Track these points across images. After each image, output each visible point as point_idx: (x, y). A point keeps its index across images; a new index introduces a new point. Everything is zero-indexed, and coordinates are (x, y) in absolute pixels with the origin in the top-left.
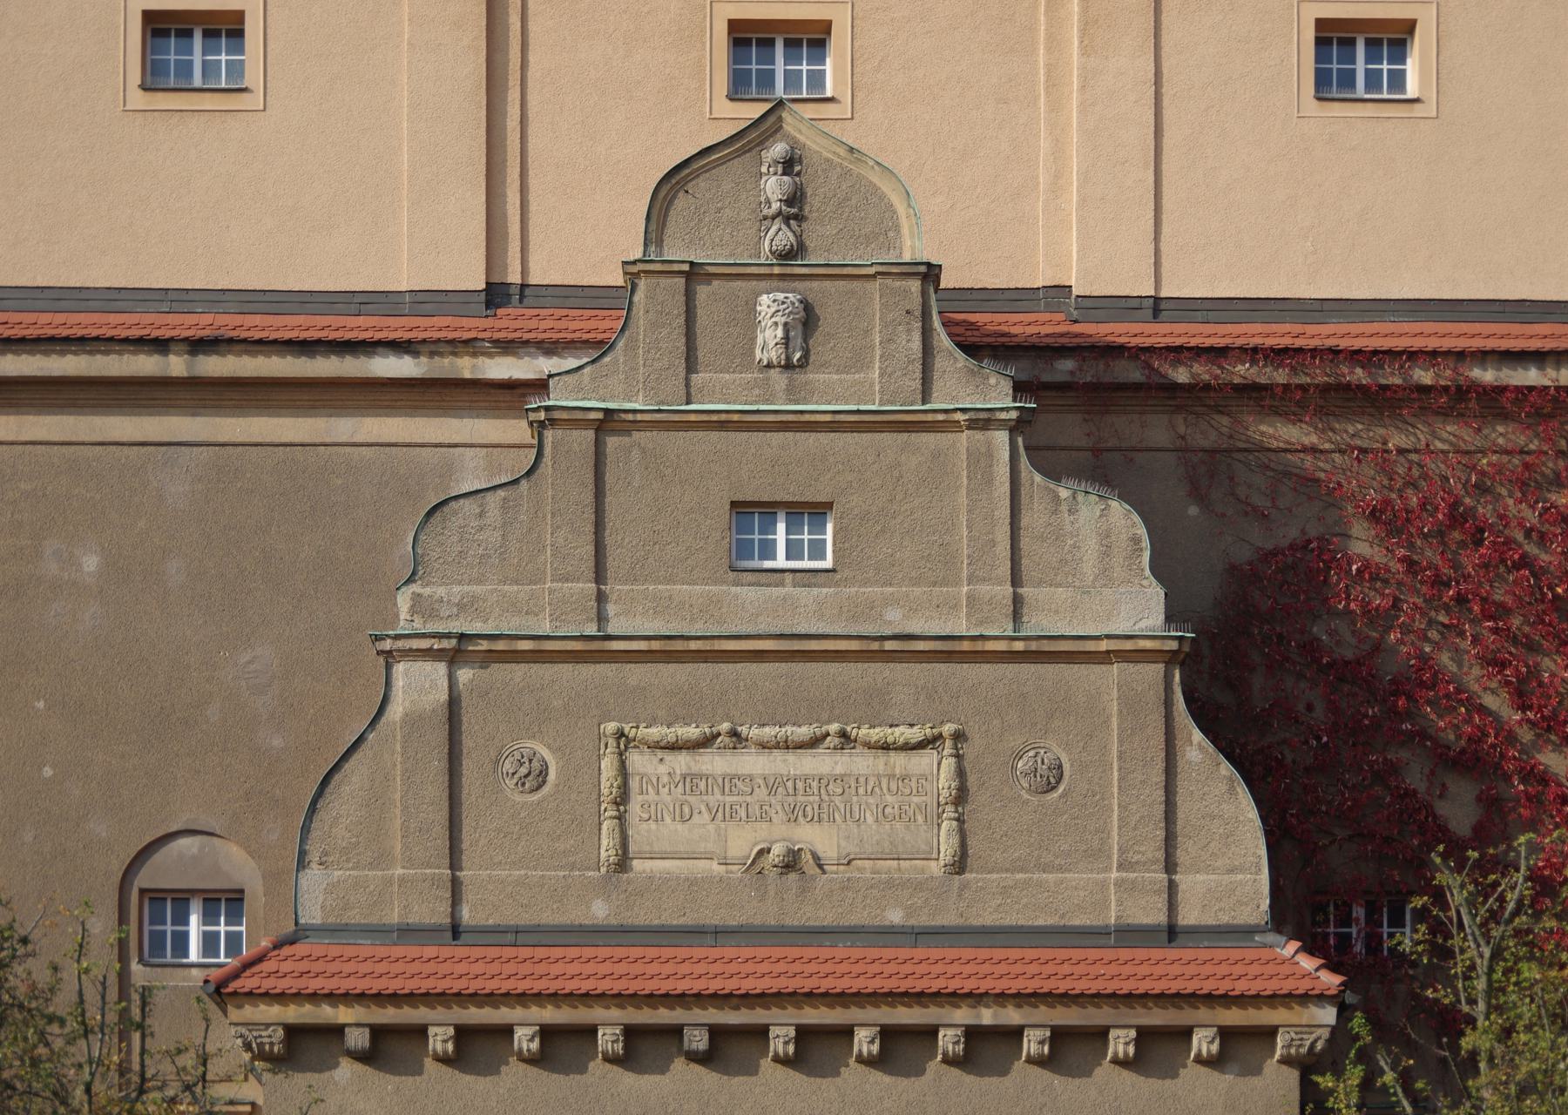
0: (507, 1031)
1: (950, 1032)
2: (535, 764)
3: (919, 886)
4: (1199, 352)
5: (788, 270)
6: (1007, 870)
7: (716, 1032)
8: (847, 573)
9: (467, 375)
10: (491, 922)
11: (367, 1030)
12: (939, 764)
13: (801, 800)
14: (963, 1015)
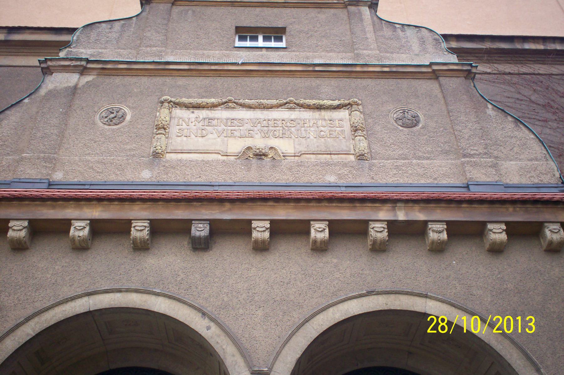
0: (66, 224)
1: (378, 225)
2: (120, 114)
3: (345, 165)
6: (397, 159)
7: (214, 224)
8: (294, 49)
10: (76, 180)
14: (384, 214)
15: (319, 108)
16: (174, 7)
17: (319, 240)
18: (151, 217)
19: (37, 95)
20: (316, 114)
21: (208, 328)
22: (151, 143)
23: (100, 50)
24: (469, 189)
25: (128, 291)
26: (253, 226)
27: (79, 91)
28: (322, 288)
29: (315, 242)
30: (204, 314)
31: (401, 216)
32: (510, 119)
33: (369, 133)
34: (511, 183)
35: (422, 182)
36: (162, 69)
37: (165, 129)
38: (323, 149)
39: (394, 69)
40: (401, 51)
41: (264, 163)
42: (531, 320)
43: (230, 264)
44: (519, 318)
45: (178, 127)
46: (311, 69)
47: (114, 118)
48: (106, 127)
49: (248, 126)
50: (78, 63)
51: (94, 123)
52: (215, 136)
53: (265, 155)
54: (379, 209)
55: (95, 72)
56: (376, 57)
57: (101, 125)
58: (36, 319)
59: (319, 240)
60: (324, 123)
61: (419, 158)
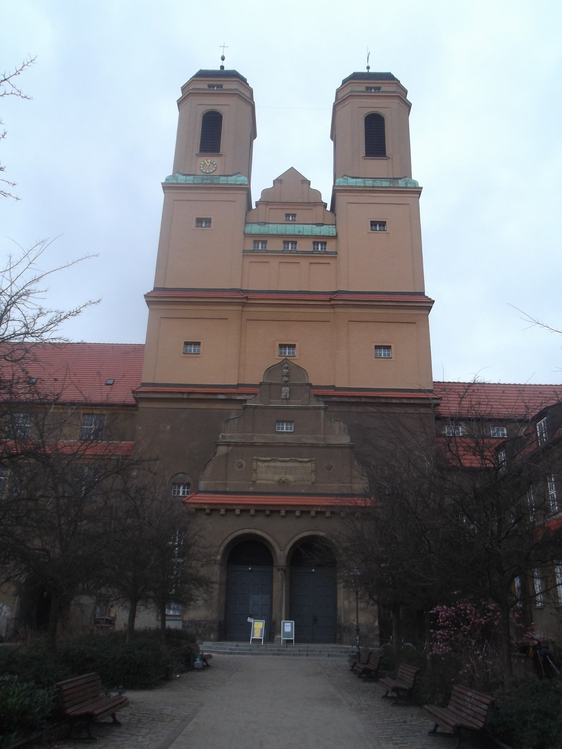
4: (356, 397)
12: (67, 695)
14: (315, 509)
15: (302, 462)
31: (319, 510)
36: (252, 445)
47: (241, 466)
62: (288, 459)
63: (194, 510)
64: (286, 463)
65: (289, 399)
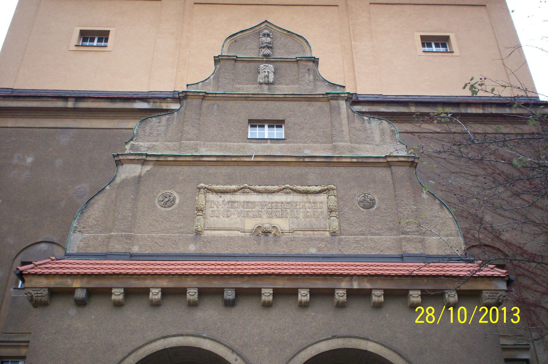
1: (341, 291)
2: (171, 198)
3: (322, 240)
5: (269, 60)
6: (357, 235)
8: (290, 140)
9: (164, 108)
10: (147, 252)
11: (85, 291)
13: (274, 210)
14: (344, 284)
15: (307, 193)
16: (204, 102)
17: (303, 302)
18: (199, 287)
19: (114, 183)
20: (304, 198)
21: (236, 360)
22: (194, 222)
23: (154, 143)
24: (403, 260)
25: (188, 335)
26: (263, 292)
27: (142, 179)
28: (304, 333)
29: (301, 302)
30: (233, 351)
31: (356, 286)
32: (437, 201)
33: (340, 213)
34: (431, 254)
35: (373, 253)
36: (197, 161)
37: (202, 211)
38: (308, 226)
39: (360, 160)
40: (367, 142)
41: (269, 239)
42: (516, 310)
43: (247, 316)
44: (504, 309)
45: (211, 209)
46: (301, 160)
47: (168, 202)
48: (163, 209)
49: (258, 208)
50: (140, 157)
51: (155, 206)
52: (236, 216)
53: (269, 232)
54: (342, 281)
55: (152, 163)
56: (348, 149)
57: (159, 207)
58: (134, 354)
59: (303, 302)
60: (310, 205)
61: (373, 234)
62: (276, 188)
63: (46, 292)
64: (270, 196)
65: (272, 84)
